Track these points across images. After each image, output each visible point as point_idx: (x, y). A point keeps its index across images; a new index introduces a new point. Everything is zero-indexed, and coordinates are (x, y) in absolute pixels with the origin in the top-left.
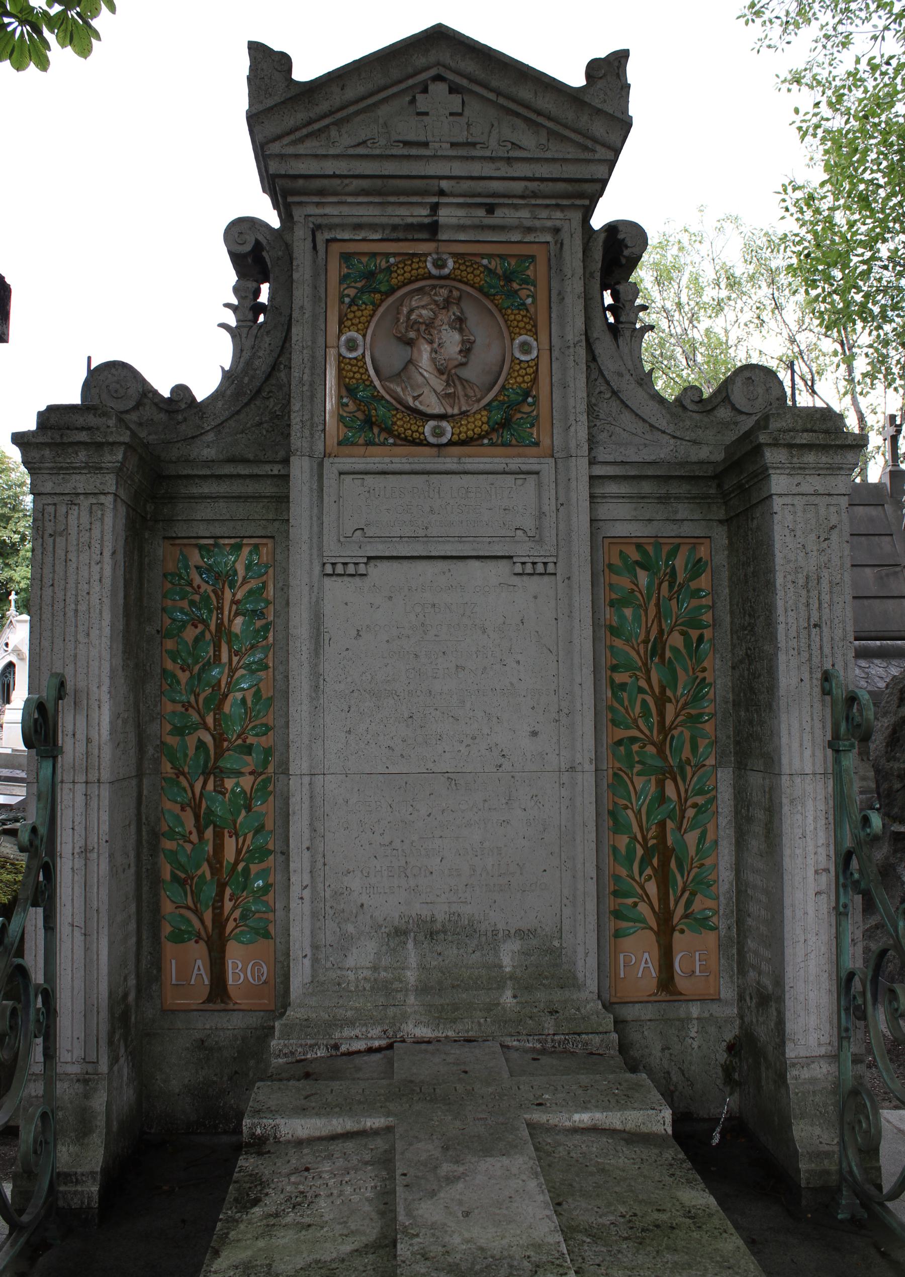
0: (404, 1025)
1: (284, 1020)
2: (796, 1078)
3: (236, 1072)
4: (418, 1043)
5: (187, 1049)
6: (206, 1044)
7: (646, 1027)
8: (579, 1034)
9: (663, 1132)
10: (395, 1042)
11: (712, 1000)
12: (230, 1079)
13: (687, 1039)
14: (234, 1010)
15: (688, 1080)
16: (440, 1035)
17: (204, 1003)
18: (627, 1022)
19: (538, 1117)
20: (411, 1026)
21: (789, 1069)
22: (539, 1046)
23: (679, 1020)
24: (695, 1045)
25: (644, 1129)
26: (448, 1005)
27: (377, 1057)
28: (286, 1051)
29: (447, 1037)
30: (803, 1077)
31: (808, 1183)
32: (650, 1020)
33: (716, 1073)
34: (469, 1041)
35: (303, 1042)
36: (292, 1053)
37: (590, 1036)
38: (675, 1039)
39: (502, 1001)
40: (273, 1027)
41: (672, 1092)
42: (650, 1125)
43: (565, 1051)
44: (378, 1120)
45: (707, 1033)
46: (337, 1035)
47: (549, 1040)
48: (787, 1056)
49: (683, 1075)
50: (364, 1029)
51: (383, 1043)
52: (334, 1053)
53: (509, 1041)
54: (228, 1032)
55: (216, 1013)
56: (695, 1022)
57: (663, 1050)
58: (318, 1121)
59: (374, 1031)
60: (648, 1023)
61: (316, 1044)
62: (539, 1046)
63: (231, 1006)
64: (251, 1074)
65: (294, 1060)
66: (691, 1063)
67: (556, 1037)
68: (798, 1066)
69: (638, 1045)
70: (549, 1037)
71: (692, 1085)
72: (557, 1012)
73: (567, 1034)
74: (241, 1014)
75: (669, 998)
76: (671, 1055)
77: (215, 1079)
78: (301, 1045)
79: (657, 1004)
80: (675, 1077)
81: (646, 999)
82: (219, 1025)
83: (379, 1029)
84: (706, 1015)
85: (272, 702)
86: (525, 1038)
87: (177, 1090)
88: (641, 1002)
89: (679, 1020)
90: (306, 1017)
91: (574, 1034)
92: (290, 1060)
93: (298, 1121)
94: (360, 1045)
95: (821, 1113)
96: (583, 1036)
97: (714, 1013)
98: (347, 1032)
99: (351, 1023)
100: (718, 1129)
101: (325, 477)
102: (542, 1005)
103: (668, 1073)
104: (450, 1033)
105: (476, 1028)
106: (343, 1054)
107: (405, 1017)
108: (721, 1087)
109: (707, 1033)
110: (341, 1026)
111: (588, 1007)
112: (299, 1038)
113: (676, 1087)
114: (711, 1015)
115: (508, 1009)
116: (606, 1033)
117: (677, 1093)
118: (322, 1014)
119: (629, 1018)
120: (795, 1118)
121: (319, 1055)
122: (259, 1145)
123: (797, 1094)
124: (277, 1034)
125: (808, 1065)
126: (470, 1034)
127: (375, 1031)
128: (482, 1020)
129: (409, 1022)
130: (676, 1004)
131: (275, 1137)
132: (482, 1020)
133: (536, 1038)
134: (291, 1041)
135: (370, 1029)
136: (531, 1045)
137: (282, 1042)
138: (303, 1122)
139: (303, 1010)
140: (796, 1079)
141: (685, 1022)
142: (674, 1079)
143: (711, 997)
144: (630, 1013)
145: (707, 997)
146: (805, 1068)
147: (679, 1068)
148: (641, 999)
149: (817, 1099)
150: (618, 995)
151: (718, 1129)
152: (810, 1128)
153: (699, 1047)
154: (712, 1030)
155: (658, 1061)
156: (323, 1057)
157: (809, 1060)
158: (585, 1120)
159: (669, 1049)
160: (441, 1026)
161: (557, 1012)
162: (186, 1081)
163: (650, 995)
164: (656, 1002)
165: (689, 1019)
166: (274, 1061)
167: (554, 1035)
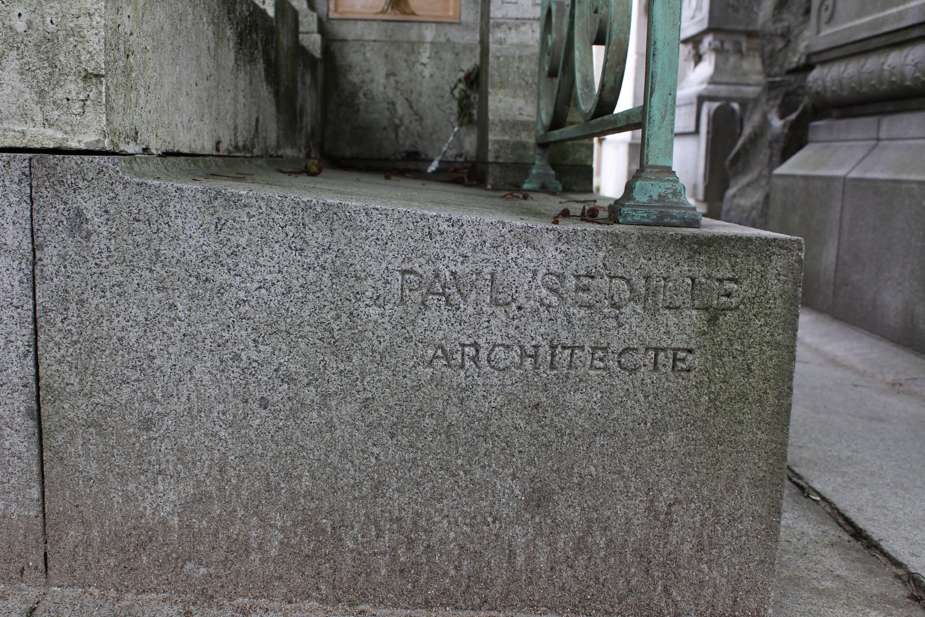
2: (501, 42)
7: (368, 48)
13: (417, 65)
15: (416, 114)
18: (346, 41)
21: (492, 30)
24: (427, 72)
30: (509, 41)
31: (497, 157)
32: (375, 41)
33: (451, 108)
38: (403, 64)
41: (397, 127)
45: (441, 59)
48: (492, 15)
49: (411, 107)
56: (428, 46)
57: (388, 76)
60: (372, 43)
68: (504, 27)
69: (358, 69)
71: (421, 119)
75: (399, 17)
76: (397, 82)
79: (385, 23)
80: (402, 109)
84: (442, 39)
85: (407, 177)
95: (527, 83)
97: (452, 39)
103: (393, 104)
113: (401, 120)
114: (448, 40)
116: (307, 33)
117: (402, 128)
119: (350, 37)
120: (493, 87)
123: (498, 58)
125: (517, 26)
130: (407, 24)
140: (501, 43)
141: (414, 46)
142: (400, 111)
143: (450, 20)
144: (348, 31)
146: (513, 31)
147: (407, 99)
148: (366, 17)
149: (524, 66)
150: (340, 10)
152: (511, 100)
153: (431, 76)
154: (448, 56)
155: (381, 89)
157: (519, 22)
159: (395, 75)
163: (377, 13)
165: (421, 42)
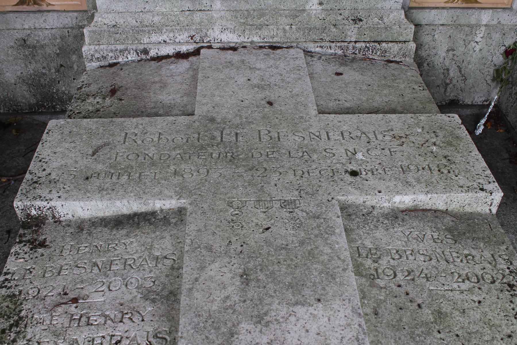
0: (210, 31)
1: (92, 27)
3: (62, 66)
4: (223, 49)
5: (12, 47)
6: (28, 43)
8: (379, 42)
9: (488, 211)
10: (202, 47)
11: (504, 8)
12: (58, 71)
14: (49, 11)
16: (246, 40)
17: (17, 5)
19: (355, 198)
20: (217, 32)
22: (340, 52)
23: (468, 26)
25: (468, 209)
26: (254, 10)
27: (184, 65)
28: (97, 55)
29: (252, 42)
34: (273, 48)
35: (113, 47)
36: (104, 58)
37: (390, 45)
38: (462, 43)
39: (307, 7)
40: (83, 35)
41: (447, 84)
42: (475, 206)
43: (365, 59)
44: (168, 202)
45: (491, 38)
46: (146, 40)
47: (351, 48)
49: (460, 71)
50: (171, 35)
51: (191, 47)
52: (144, 57)
53: (312, 47)
54: (47, 32)
55: (31, 15)
56: (483, 29)
57: (448, 51)
58: (99, 203)
59: (182, 37)
60: (441, 28)
61: (126, 50)
62: (340, 52)
63: (45, 7)
64: (75, 67)
65: (107, 63)
66: (469, 63)
67: (358, 45)
69: (427, 46)
70: (351, 45)
72: (361, 20)
73: (368, 42)
74: (55, 15)
76: (454, 55)
77: (44, 71)
78: (112, 51)
79: (453, 11)
81: (443, 5)
82: (37, 25)
83: (186, 34)
86: (328, 44)
87: (13, 81)
88: (437, 8)
89: (468, 26)
90: (114, 23)
91: (374, 42)
92: (103, 63)
93: (77, 203)
94: (168, 50)
96: (384, 44)
98: (155, 38)
99: (157, 29)
100: (483, 121)
101: (335, 115)
102: (346, 13)
103: (448, 70)
104: (256, 39)
105: (281, 34)
106: (153, 59)
107: (211, 22)
108: (489, 82)
109: (491, 38)
110: (149, 32)
111: (391, 16)
112: (109, 44)
114: (499, 23)
115: (313, 16)
116: (405, 42)
117: (451, 86)
118: (130, 19)
119: (423, 22)
121: (130, 59)
122: (34, 231)
124: (87, 40)
126: (275, 40)
127: (183, 37)
128: (287, 27)
129: (216, 28)
131: (54, 217)
132: (287, 27)
133: (338, 44)
134: (102, 47)
135: (177, 35)
136: (332, 51)
137: (92, 47)
138: (82, 204)
139: (110, 16)
141: (473, 27)
142: (451, 74)
144: (424, 17)
145: (499, 6)
147: (458, 66)
151: (483, 121)
154: (496, 36)
155: (441, 60)
156: (133, 61)
158: (407, 202)
159: (454, 50)
160: (247, 32)
161: (361, 20)
162: (19, 73)
164: (451, 8)
166: (88, 65)
167: (356, 42)
